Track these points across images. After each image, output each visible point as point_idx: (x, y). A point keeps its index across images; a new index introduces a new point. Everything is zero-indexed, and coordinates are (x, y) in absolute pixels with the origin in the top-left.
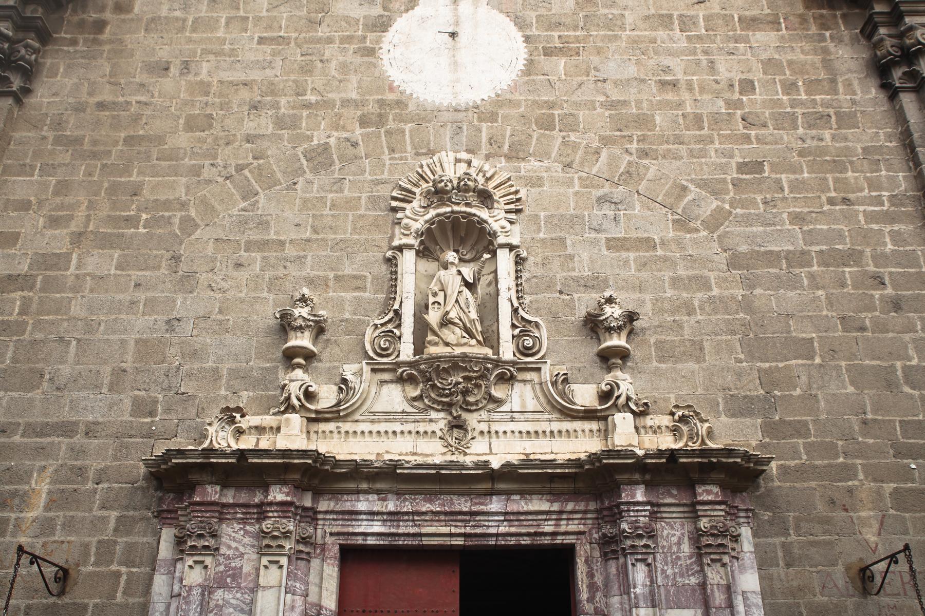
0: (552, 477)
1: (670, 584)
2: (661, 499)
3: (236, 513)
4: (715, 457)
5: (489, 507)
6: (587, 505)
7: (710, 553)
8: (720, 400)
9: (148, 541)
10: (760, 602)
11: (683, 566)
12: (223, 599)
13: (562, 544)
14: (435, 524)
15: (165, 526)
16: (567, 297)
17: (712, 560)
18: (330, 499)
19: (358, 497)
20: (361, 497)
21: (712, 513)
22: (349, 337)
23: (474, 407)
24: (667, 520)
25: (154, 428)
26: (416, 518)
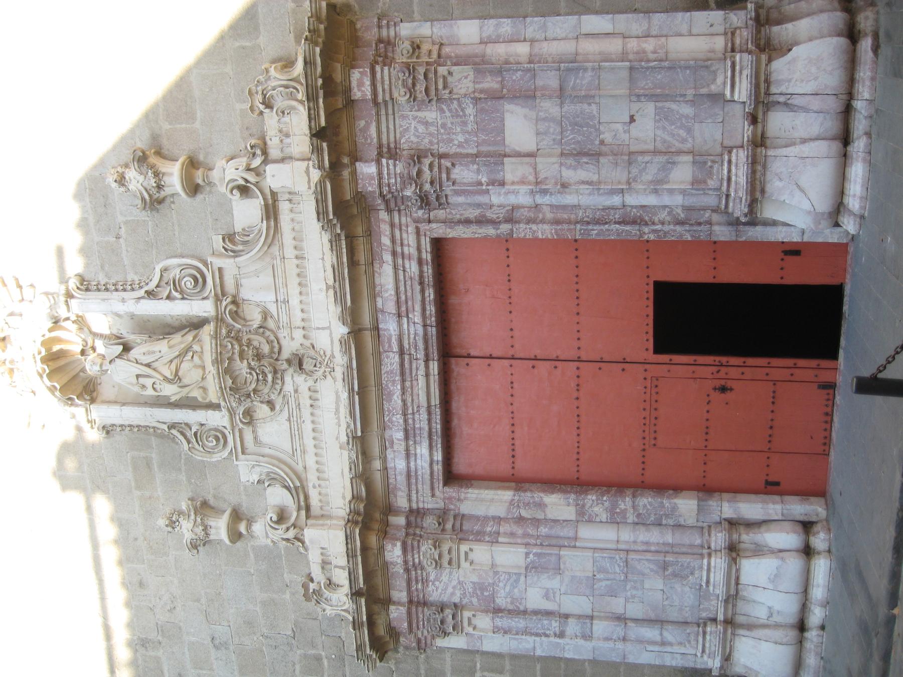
0: (353, 263)
1: (476, 139)
2: (372, 141)
3: (417, 590)
4: (316, 82)
5: (393, 333)
6: (384, 221)
7: (437, 89)
8: (237, 44)
9: (450, 656)
10: (492, 22)
11: (454, 121)
12: (506, 598)
13: (432, 252)
14: (415, 391)
15: (433, 643)
16: (123, 230)
17: (445, 87)
18: (396, 496)
19: (391, 468)
20: (390, 465)
21: (387, 82)
22: (208, 476)
23: (276, 344)
24: (398, 135)
25: (333, 656)
26: (410, 411)
